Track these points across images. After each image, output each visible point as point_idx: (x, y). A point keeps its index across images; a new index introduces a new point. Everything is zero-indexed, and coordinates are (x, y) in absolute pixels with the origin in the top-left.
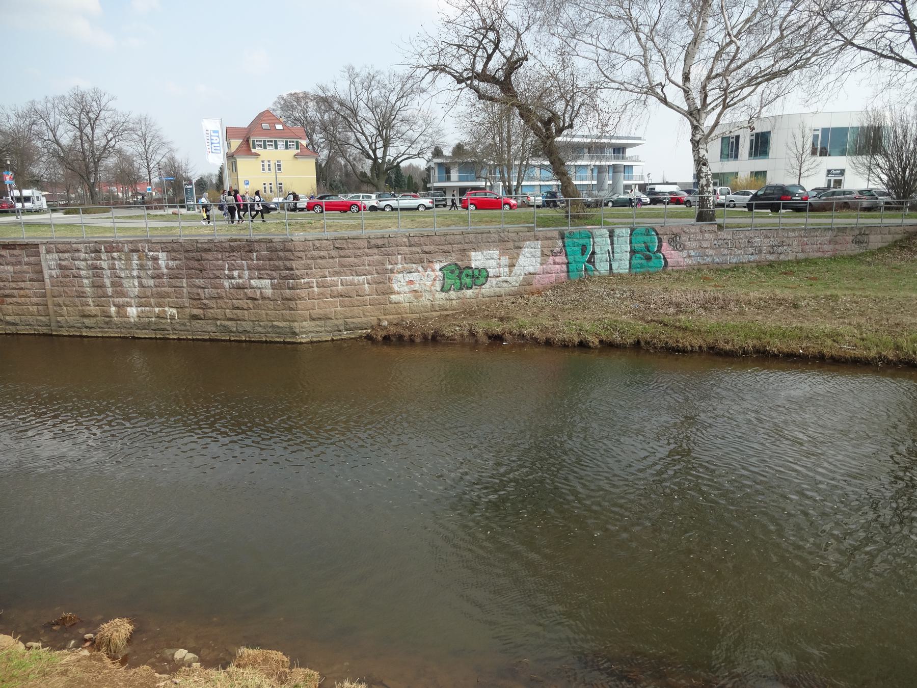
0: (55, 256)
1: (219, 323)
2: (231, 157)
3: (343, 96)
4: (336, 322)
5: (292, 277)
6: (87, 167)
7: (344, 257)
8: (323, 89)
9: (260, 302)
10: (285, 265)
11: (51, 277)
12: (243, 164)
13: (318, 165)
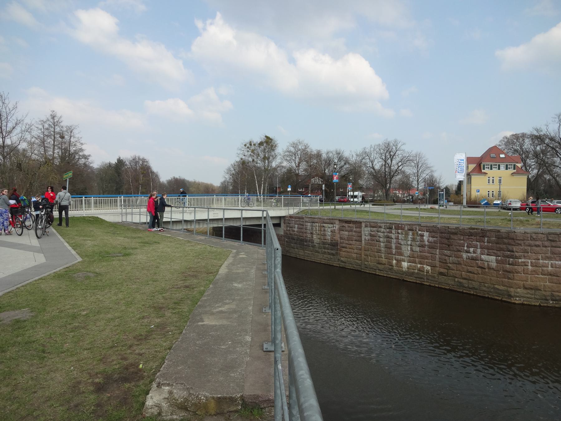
0: (369, 229)
1: (456, 279)
2: (469, 175)
3: (553, 134)
4: (544, 293)
5: (512, 257)
6: (386, 180)
7: (556, 247)
8: (537, 130)
9: (487, 270)
10: (508, 248)
11: (365, 240)
12: (475, 179)
13: (528, 179)
